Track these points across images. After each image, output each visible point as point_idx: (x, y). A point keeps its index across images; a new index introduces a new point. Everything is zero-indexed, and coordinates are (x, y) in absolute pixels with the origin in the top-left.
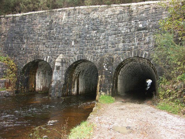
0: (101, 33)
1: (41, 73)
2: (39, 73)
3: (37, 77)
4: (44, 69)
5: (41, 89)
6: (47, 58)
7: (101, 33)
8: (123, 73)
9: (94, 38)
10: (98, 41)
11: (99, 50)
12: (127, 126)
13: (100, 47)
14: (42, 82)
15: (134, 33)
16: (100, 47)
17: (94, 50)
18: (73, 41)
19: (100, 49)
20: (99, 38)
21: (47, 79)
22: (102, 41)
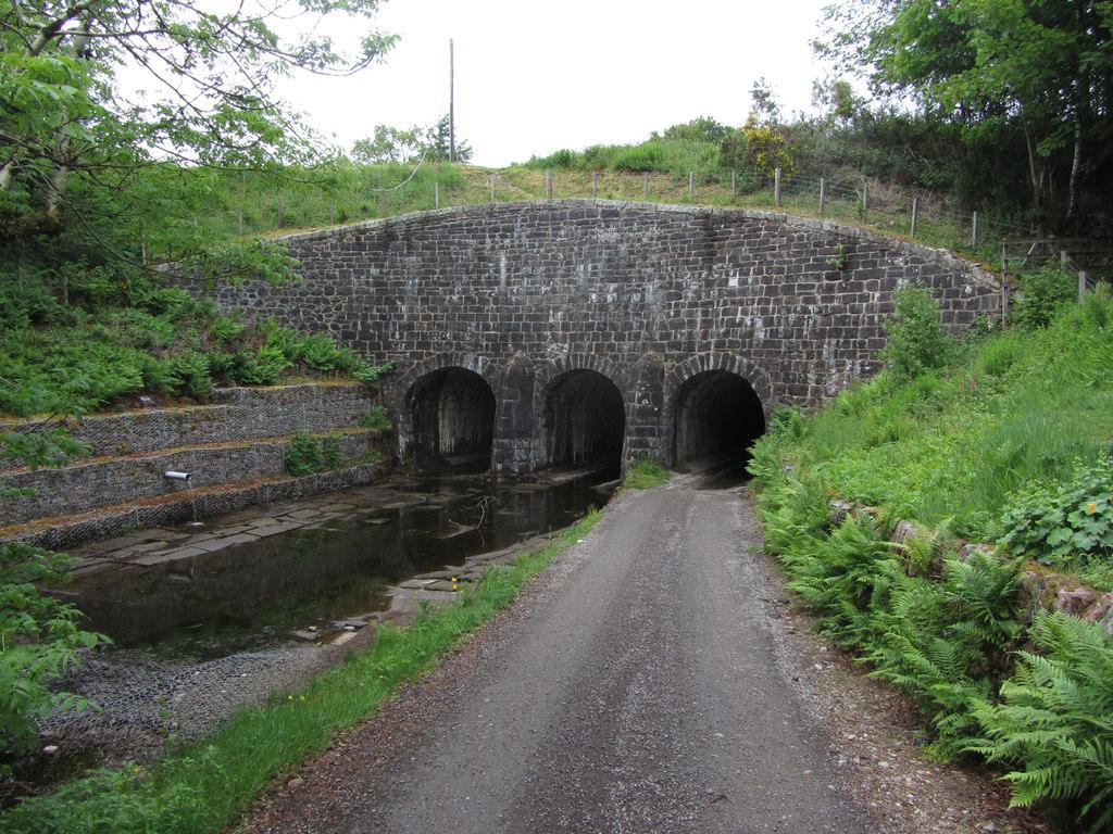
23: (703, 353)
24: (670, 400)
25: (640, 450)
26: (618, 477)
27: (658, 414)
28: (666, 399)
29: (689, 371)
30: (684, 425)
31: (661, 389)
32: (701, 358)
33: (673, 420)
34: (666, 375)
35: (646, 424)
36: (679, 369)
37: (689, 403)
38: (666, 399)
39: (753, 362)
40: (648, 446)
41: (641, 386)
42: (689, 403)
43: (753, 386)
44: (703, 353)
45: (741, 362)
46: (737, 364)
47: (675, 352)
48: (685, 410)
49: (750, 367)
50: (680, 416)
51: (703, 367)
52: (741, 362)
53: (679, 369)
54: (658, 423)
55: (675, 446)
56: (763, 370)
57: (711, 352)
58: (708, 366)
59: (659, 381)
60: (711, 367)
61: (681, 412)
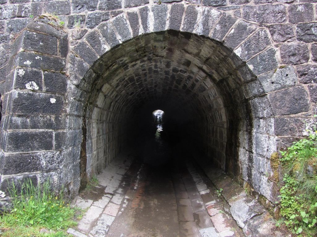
23: (136, 10)
24: (77, 86)
25: (19, 176)
26: (175, 68)
27: (57, 109)
28: (71, 85)
29: (110, 38)
30: (94, 130)
31: (62, 68)
32: (133, 17)
33: (81, 121)
34: (71, 47)
35: (34, 126)
36: (93, 38)
37: (100, 101)
38: (71, 85)
39: (231, 13)
40: (37, 167)
41: (24, 57)
42: (100, 101)
43: (238, 52)
44: (136, 10)
45: (207, 16)
46: (200, 19)
47: (86, 13)
48: (96, 110)
49: (226, 22)
50: (90, 117)
51: (135, 29)
52: (207, 16)
53: (93, 38)
54: (58, 125)
55: (83, 158)
56: (253, 25)
57: (149, 6)
58: (145, 27)
59: (59, 56)
60: (151, 29)
61: (92, 111)
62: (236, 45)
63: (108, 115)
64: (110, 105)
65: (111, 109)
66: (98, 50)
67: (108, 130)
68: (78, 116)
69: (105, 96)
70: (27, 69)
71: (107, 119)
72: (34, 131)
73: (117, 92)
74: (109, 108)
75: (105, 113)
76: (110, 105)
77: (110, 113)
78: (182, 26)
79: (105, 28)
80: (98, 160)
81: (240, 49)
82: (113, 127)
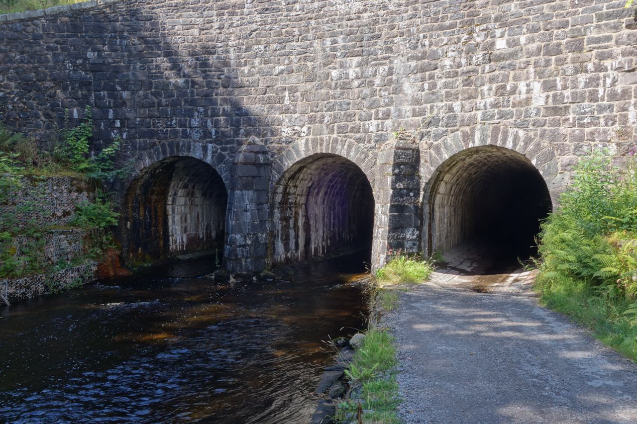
0: (376, 65)
1: (181, 192)
2: (175, 194)
3: (561, 356)
4: (189, 180)
5: (183, 246)
6: (205, 149)
7: (376, 65)
8: (449, 186)
9: (356, 83)
10: (367, 91)
11: (375, 122)
12: (421, 149)
13: (377, 113)
14: (186, 220)
15: (480, 69)
16: (377, 113)
17: (358, 122)
18: (287, 93)
19: (376, 119)
20: (371, 83)
21: (199, 209)
22: (383, 93)
39: (532, 134)
62: (532, 156)
63: (448, 199)
64: (451, 189)
65: (452, 193)
66: (441, 158)
67: (449, 214)
68: (265, 168)
69: (446, 183)
70: (227, 45)
71: (448, 203)
72: (302, 219)
73: (458, 176)
74: (450, 192)
75: (447, 197)
76: (451, 189)
77: (451, 197)
78: (499, 142)
79: (446, 141)
80: (440, 241)
81: (535, 160)
82: (455, 211)
